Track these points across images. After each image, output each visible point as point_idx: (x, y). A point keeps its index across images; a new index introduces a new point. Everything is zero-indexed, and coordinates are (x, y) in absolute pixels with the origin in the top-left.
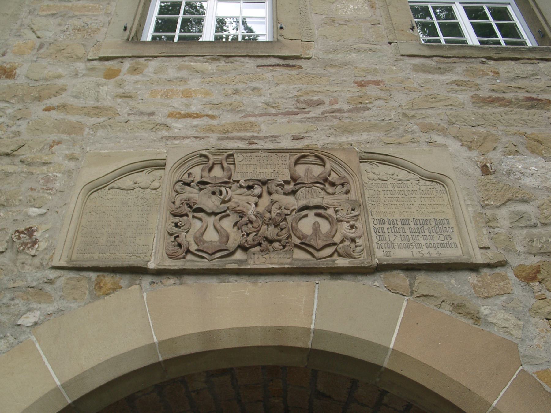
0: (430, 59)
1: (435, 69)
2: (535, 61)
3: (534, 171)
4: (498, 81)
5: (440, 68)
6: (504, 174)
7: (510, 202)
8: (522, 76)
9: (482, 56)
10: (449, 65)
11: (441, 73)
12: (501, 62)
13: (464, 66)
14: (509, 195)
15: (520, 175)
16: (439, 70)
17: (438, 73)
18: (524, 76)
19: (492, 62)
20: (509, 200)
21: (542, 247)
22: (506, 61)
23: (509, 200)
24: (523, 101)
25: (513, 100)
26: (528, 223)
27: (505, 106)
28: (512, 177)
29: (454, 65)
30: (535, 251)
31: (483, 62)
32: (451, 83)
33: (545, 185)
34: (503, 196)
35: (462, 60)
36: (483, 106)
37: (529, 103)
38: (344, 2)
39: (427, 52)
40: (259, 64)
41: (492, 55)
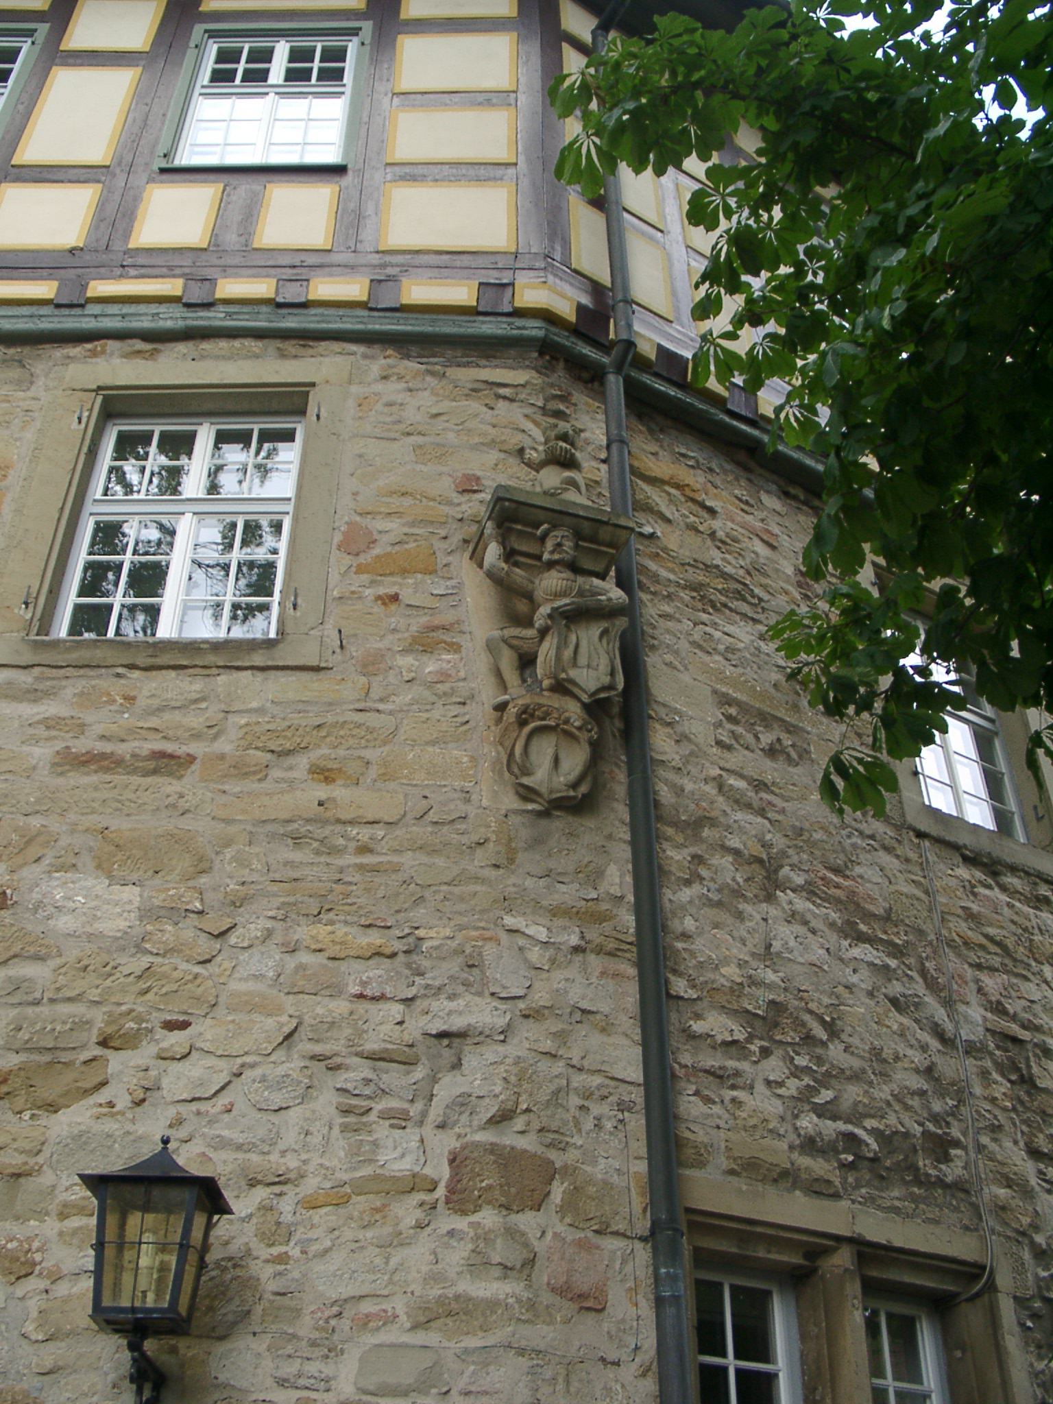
0: (26, 671)
1: (28, 691)
2: (215, 671)
3: (79, 905)
4: (126, 716)
5: (36, 690)
6: (28, 909)
7: (16, 960)
8: (173, 704)
9: (121, 662)
10: (55, 682)
11: (35, 701)
12: (154, 673)
13: (80, 685)
14: (16, 949)
15: (53, 910)
16: (33, 695)
17: (29, 701)
18: (178, 704)
19: (136, 674)
20: (15, 956)
21: (31, 1039)
22: (163, 672)
23: (15, 956)
24: (147, 759)
25: (128, 757)
26: (25, 998)
27: (107, 770)
28: (41, 914)
29: (64, 683)
30: (17, 1045)
31: (118, 675)
32: (38, 722)
33: (89, 929)
34: (8, 948)
35: (82, 671)
36: (69, 771)
37: (151, 765)
38: (923, 47)
39: (27, 658)
40: (659, 234)
41: (141, 661)
